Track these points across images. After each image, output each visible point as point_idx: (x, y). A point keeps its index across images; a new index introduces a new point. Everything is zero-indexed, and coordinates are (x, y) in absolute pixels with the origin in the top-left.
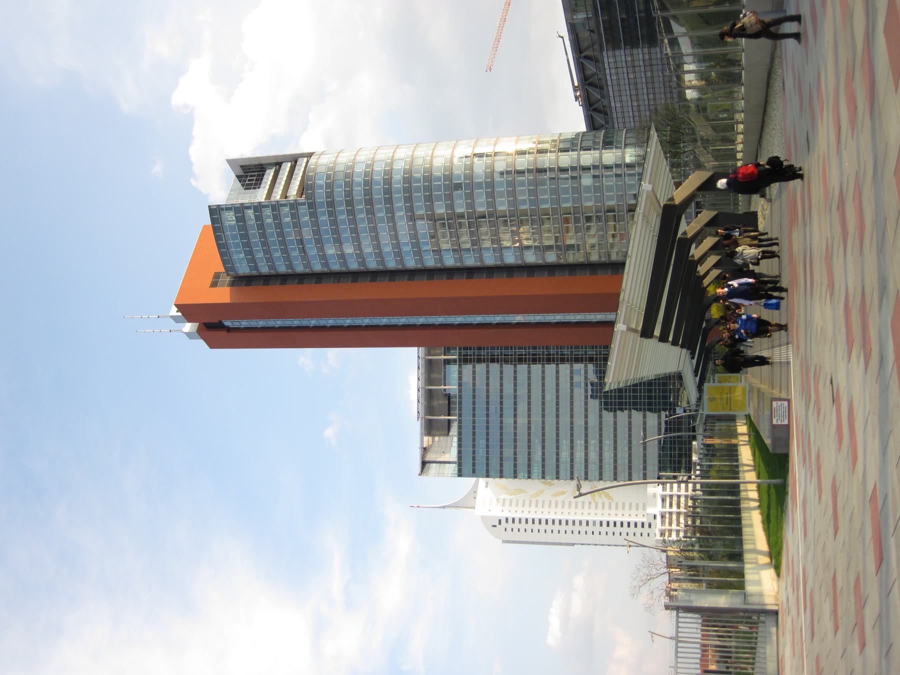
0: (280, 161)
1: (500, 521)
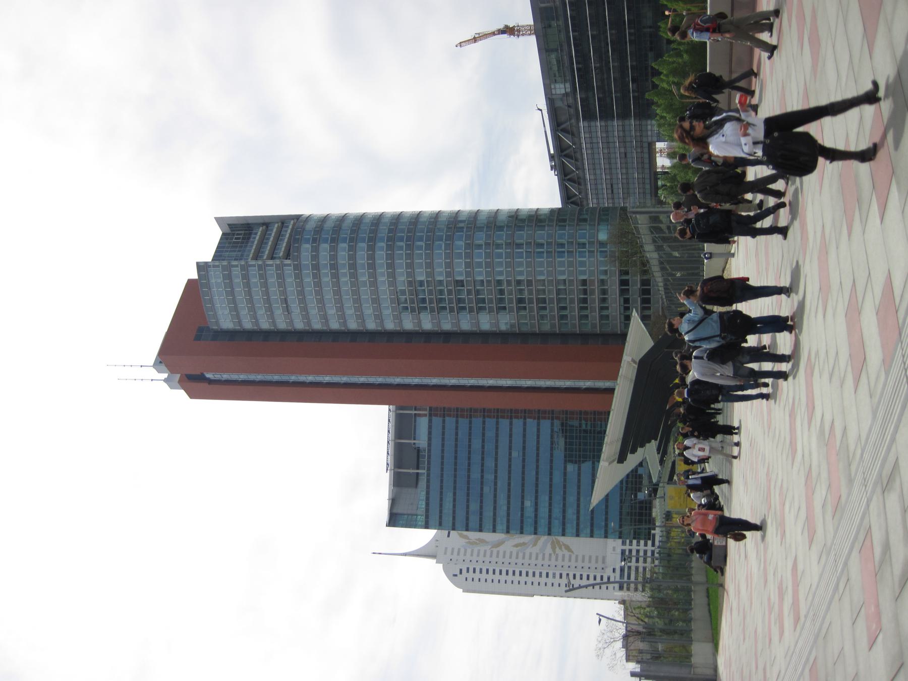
0: (267, 221)
1: (461, 570)
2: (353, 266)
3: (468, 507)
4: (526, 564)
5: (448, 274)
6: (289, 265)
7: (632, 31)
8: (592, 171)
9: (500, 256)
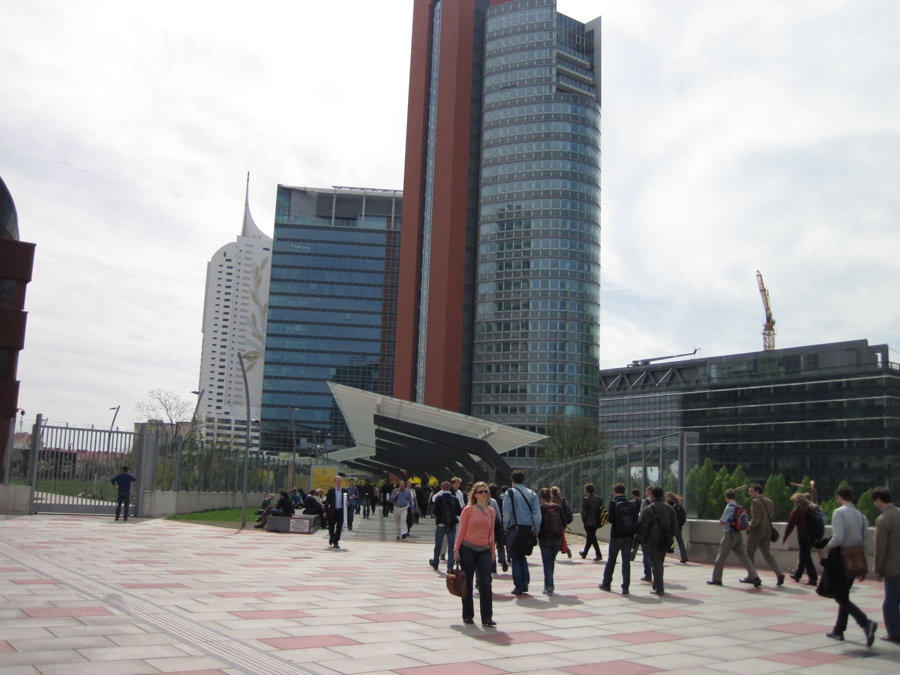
0: (595, 70)
1: (230, 260)
2: (547, 156)
3: (296, 267)
4: (234, 326)
5: (536, 253)
6: (550, 91)
7: (773, 447)
8: (631, 402)
9: (553, 306)
